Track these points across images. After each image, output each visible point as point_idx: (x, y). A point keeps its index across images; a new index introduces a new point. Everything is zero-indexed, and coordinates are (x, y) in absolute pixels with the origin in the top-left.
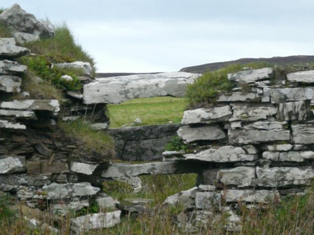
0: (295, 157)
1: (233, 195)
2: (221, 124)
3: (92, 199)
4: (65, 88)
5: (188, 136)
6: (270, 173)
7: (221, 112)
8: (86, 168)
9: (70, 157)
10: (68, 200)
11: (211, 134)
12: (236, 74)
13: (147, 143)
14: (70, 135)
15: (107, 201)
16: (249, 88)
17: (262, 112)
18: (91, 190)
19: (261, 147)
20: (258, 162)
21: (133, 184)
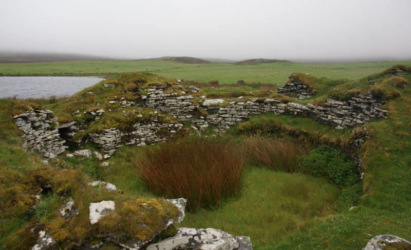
0: (238, 117)
1: (227, 122)
2: (226, 111)
3: (204, 122)
4: (200, 103)
5: (221, 112)
6: (234, 119)
7: (226, 109)
8: (202, 117)
9: (201, 115)
10: (199, 122)
11: (224, 112)
12: (95, 217)
13: (214, 111)
14: (242, 191)
15: (206, 123)
16: (231, 105)
17: (233, 109)
18: (203, 121)
19: (233, 115)
20: (232, 117)
21: (141, 181)
